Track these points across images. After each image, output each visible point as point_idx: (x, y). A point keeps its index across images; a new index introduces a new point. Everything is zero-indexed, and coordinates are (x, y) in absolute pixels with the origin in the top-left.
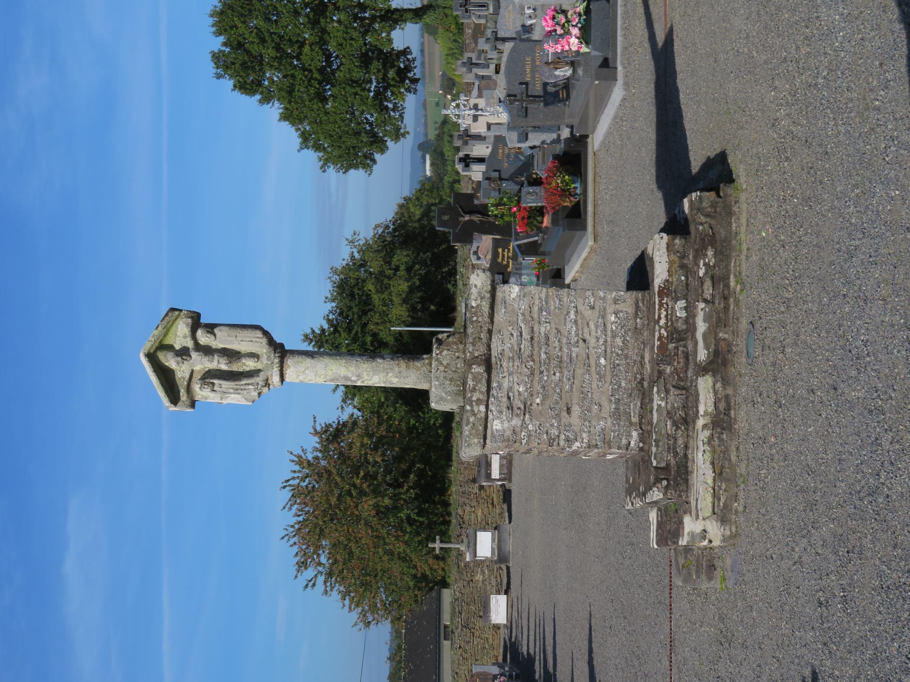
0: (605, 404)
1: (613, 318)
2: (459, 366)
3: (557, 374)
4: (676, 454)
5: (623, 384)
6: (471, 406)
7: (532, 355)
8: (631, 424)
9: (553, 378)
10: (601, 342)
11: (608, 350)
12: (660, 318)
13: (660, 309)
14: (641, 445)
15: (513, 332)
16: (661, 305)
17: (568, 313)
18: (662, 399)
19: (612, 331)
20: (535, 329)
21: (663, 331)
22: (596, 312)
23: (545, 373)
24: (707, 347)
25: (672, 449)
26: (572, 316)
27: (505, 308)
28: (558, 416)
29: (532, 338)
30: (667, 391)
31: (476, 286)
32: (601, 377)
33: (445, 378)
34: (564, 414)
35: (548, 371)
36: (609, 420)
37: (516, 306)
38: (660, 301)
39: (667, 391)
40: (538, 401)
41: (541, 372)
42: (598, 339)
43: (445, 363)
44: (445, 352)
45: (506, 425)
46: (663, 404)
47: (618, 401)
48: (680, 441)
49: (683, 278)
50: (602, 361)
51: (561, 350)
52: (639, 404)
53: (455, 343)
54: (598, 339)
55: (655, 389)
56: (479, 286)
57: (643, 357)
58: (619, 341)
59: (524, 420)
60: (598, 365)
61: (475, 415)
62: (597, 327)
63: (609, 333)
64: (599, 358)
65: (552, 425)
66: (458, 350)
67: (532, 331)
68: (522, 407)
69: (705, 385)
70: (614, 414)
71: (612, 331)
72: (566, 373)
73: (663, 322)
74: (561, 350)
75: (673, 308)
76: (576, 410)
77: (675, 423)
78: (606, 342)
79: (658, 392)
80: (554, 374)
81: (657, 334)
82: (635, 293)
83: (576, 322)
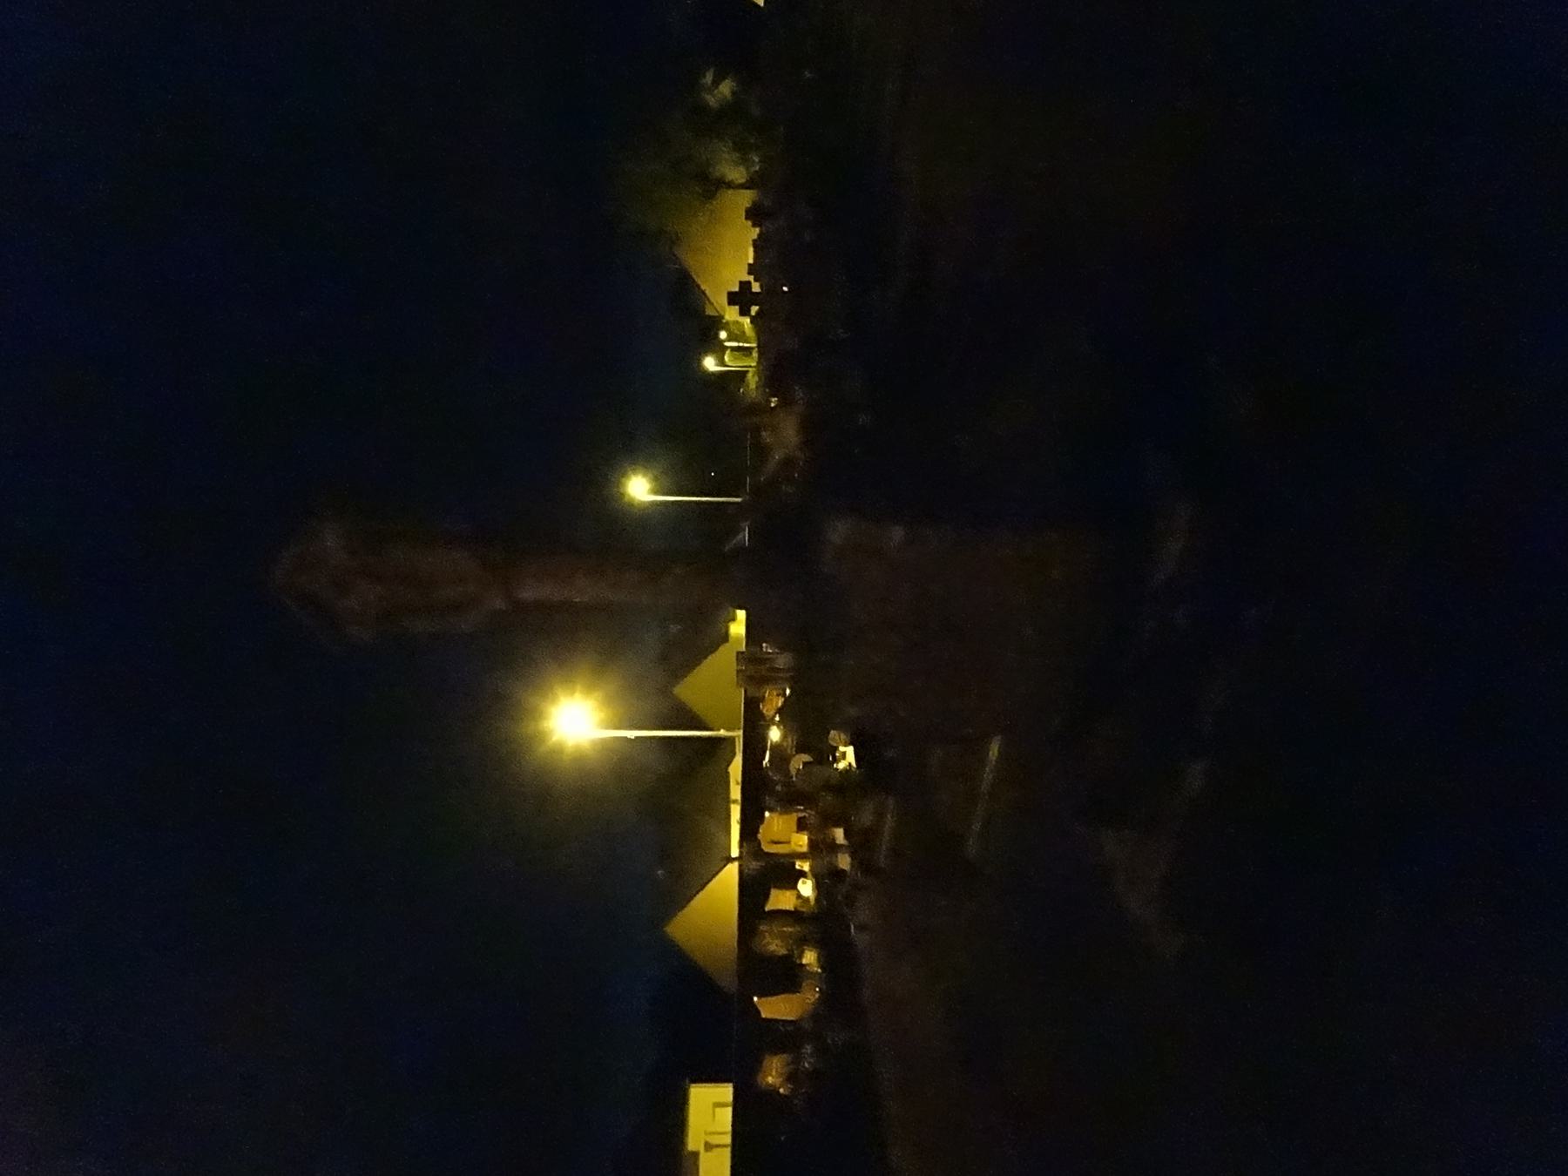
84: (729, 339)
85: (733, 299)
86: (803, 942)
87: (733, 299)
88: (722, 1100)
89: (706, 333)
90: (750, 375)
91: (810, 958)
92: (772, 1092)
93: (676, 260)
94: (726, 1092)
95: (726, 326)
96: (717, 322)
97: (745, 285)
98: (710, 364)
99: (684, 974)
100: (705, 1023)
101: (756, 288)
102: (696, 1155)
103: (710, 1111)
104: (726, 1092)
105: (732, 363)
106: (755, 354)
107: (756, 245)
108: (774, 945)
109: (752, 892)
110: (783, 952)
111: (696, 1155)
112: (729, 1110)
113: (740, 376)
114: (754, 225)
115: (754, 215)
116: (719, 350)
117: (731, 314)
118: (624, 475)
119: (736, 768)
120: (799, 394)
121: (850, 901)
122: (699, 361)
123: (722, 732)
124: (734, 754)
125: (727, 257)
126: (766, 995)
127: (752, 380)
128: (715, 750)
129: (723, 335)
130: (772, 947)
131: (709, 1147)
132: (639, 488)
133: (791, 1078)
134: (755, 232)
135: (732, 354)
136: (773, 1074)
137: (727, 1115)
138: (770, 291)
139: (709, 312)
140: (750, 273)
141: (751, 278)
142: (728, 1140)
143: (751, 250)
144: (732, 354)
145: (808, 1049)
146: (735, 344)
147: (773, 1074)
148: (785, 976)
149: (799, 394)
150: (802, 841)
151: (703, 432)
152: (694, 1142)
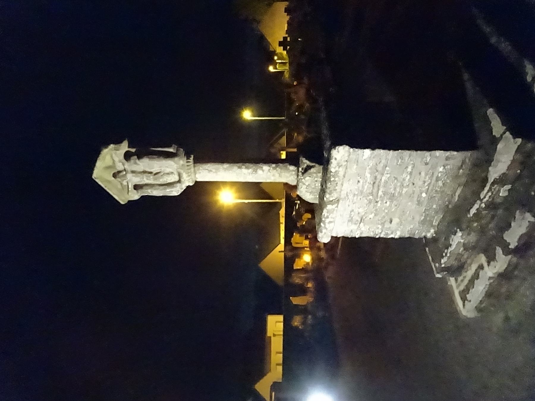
2: (317, 185)
3: (388, 203)
6: (325, 224)
9: (385, 204)
13: (488, 192)
14: (434, 235)
15: (360, 180)
17: (407, 167)
19: (437, 177)
20: (378, 177)
22: (429, 166)
23: (380, 202)
24: (479, 309)
26: (409, 169)
27: (357, 165)
28: (383, 224)
29: (374, 183)
31: (336, 159)
32: (419, 203)
33: (306, 191)
35: (382, 201)
37: (366, 163)
41: (377, 202)
42: (424, 182)
43: (307, 184)
44: (307, 178)
49: (519, 171)
50: (424, 195)
51: (395, 189)
52: (442, 216)
53: (315, 173)
54: (424, 182)
56: (338, 159)
58: (440, 183)
60: (420, 196)
61: (326, 229)
62: (426, 174)
63: (434, 178)
66: (317, 177)
67: (376, 178)
68: (359, 220)
71: (437, 177)
74: (395, 189)
80: (386, 203)
81: (476, 206)
83: (411, 173)
84: (278, 59)
85: (281, 44)
86: (307, 280)
87: (281, 44)
88: (279, 320)
89: (269, 57)
90: (285, 73)
91: (310, 285)
92: (297, 327)
93: (259, 31)
94: (281, 318)
95: (276, 55)
96: (274, 53)
97: (285, 38)
98: (271, 69)
99: (265, 279)
100: (274, 295)
101: (289, 39)
102: (270, 337)
103: (275, 324)
104: (281, 318)
105: (279, 69)
106: (288, 65)
107: (288, 23)
108: (297, 280)
109: (289, 261)
110: (300, 282)
111: (270, 337)
112: (282, 324)
113: (281, 73)
114: (288, 15)
115: (287, 10)
116: (274, 64)
117: (280, 50)
118: (220, 211)
119: (282, 212)
120: (306, 80)
121: (326, 268)
122: (268, 67)
123: (277, 200)
124: (281, 208)
125: (277, 28)
126: (294, 297)
127: (287, 75)
128: (277, 206)
129: (276, 58)
130: (297, 281)
131: (274, 335)
132: (247, 115)
133: (304, 323)
134: (287, 18)
135: (280, 65)
136: (297, 321)
137: (281, 325)
138: (294, 40)
139: (271, 49)
140: (286, 34)
141: (287, 36)
142: (282, 333)
143: (286, 25)
144: (280, 65)
145: (310, 317)
146: (280, 61)
147: (297, 321)
148: (302, 291)
149: (306, 80)
150: (306, 243)
151: (271, 94)
152: (269, 333)
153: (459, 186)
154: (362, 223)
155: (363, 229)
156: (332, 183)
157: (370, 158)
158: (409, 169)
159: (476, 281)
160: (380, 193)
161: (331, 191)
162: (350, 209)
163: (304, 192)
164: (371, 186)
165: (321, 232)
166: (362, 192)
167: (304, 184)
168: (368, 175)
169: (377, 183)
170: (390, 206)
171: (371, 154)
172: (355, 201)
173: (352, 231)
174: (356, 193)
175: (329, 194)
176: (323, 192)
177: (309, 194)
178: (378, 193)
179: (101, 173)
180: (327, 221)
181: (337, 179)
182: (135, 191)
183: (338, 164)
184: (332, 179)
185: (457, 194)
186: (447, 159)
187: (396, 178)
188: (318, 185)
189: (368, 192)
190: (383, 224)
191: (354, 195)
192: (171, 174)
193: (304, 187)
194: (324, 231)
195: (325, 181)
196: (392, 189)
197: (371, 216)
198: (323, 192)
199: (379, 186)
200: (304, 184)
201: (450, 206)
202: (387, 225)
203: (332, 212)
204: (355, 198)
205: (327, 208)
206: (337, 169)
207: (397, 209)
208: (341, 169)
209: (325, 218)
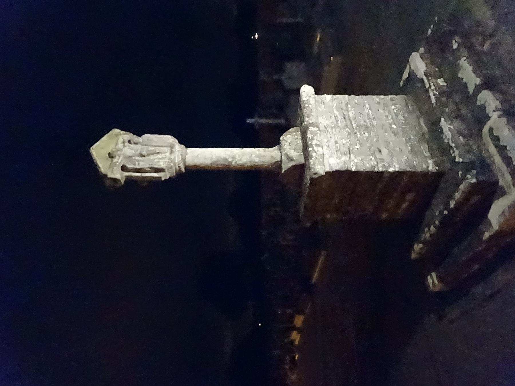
0: (403, 147)
1: (393, 107)
4: (475, 154)
5: (412, 137)
6: (313, 147)
7: (347, 125)
8: (426, 157)
9: (364, 135)
10: (390, 118)
11: (395, 122)
12: (430, 86)
16: (429, 81)
17: (364, 106)
18: (450, 125)
21: (435, 92)
23: (358, 133)
25: (470, 151)
26: (367, 106)
29: (345, 118)
30: (452, 121)
32: (395, 134)
34: (377, 153)
35: (359, 132)
36: (410, 156)
38: (427, 79)
39: (452, 121)
40: (357, 147)
45: (338, 161)
46: (452, 127)
47: (412, 146)
48: (474, 147)
50: (394, 126)
51: (365, 121)
54: (387, 116)
55: (443, 119)
57: (419, 124)
59: (350, 157)
60: (391, 128)
63: (394, 115)
64: (391, 124)
65: (371, 159)
67: (344, 114)
68: (347, 150)
69: (488, 100)
70: (412, 152)
72: (372, 133)
73: (433, 87)
74: (365, 121)
75: (437, 82)
76: (385, 151)
77: (464, 137)
78: (392, 118)
79: (445, 121)
80: (364, 133)
82: (404, 96)
153: (419, 119)
154: (352, 155)
155: (356, 161)
156: (307, 108)
157: (332, 100)
158: (367, 106)
159: (502, 144)
160: (354, 125)
161: (308, 115)
162: (333, 140)
163: (288, 149)
164: (344, 120)
165: (312, 157)
166: (338, 127)
167: (287, 142)
168: (337, 113)
169: (347, 117)
170: (370, 135)
171: (332, 97)
172: (335, 133)
173: (345, 163)
174: (333, 126)
175: (308, 117)
176: (305, 147)
177: (293, 151)
178: (352, 125)
179: (99, 151)
180: (314, 142)
181: (310, 106)
182: (120, 170)
183: (308, 95)
184: (307, 105)
185: (423, 124)
186: (392, 100)
187: (361, 114)
188: (300, 142)
189: (343, 125)
190: (373, 154)
191: (332, 128)
192: (164, 155)
193: (287, 144)
194: (314, 154)
195: (304, 135)
196: (363, 122)
197: (357, 147)
198: (305, 147)
199: (350, 120)
200: (287, 142)
201: (427, 136)
202: (379, 156)
203: (316, 134)
204: (334, 130)
205: (310, 130)
206: (308, 98)
207: (378, 138)
208: (311, 99)
209: (311, 140)
